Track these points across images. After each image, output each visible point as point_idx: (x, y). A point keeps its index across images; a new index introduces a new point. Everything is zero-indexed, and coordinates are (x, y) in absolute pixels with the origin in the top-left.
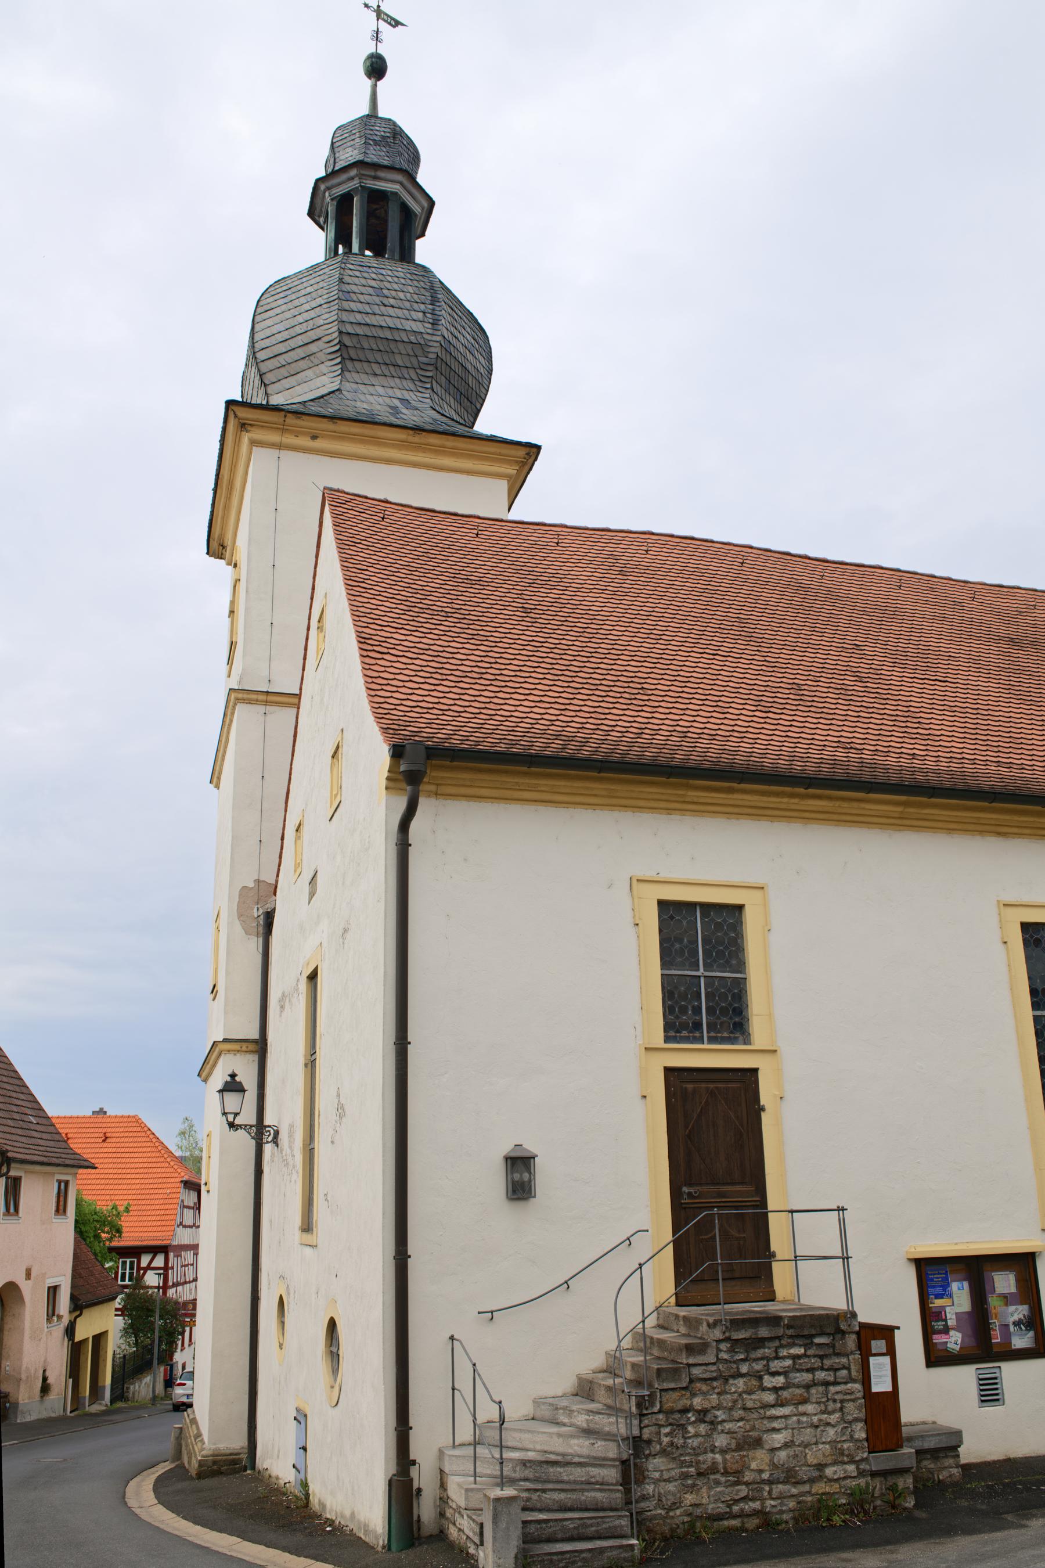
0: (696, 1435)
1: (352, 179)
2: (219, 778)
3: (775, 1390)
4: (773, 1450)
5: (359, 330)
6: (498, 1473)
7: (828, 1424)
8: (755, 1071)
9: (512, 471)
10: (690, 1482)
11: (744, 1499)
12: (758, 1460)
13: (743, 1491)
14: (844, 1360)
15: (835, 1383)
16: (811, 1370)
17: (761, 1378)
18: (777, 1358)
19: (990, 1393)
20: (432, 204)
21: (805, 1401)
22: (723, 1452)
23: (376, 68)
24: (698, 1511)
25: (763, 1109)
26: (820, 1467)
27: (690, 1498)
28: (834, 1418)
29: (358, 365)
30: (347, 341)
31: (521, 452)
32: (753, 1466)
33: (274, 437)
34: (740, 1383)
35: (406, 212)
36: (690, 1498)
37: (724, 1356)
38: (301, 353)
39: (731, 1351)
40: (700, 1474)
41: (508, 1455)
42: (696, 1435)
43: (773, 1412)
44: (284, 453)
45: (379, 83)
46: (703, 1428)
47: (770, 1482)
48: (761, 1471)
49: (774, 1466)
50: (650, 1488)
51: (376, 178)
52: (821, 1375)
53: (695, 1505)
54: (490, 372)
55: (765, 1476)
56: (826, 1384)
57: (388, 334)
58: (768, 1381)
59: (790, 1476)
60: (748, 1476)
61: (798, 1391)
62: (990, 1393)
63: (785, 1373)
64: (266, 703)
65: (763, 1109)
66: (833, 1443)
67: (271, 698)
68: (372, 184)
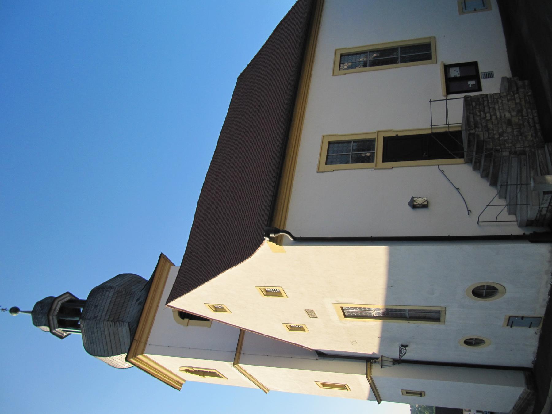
0: (508, 136)
1: (53, 319)
2: (266, 388)
3: (491, 116)
4: (512, 116)
5: (109, 314)
6: (525, 206)
7: (502, 102)
8: (384, 138)
9: (168, 264)
10: (524, 138)
11: (529, 122)
12: (515, 120)
13: (526, 123)
14: (481, 98)
15: (488, 101)
16: (484, 107)
17: (487, 120)
18: (480, 115)
19: (489, 75)
20: (68, 293)
21: (494, 109)
22: (513, 129)
23: (15, 310)
24: (534, 135)
25: (397, 135)
26: (516, 104)
27: (530, 138)
28: (500, 101)
29: (121, 316)
30: (111, 319)
31: (162, 259)
32: (517, 121)
33: (142, 345)
34: (490, 126)
35: (70, 301)
36: (530, 138)
37: (480, 130)
38: (112, 338)
39: (479, 128)
40: (521, 135)
41: (519, 203)
42: (508, 136)
43: (498, 116)
44: (148, 342)
45: (21, 310)
46: (505, 135)
47: (522, 116)
48: (519, 119)
49: (517, 116)
50: (528, 149)
51: (55, 310)
52: (486, 103)
53: (532, 137)
54: (131, 274)
55: (520, 118)
56: (488, 103)
57: (112, 304)
58: (488, 117)
59: (520, 112)
60: (521, 122)
61: (491, 110)
62: (489, 75)
63: (485, 114)
64: (240, 353)
65: (397, 135)
66: (508, 100)
67: (238, 351)
68: (56, 312)
